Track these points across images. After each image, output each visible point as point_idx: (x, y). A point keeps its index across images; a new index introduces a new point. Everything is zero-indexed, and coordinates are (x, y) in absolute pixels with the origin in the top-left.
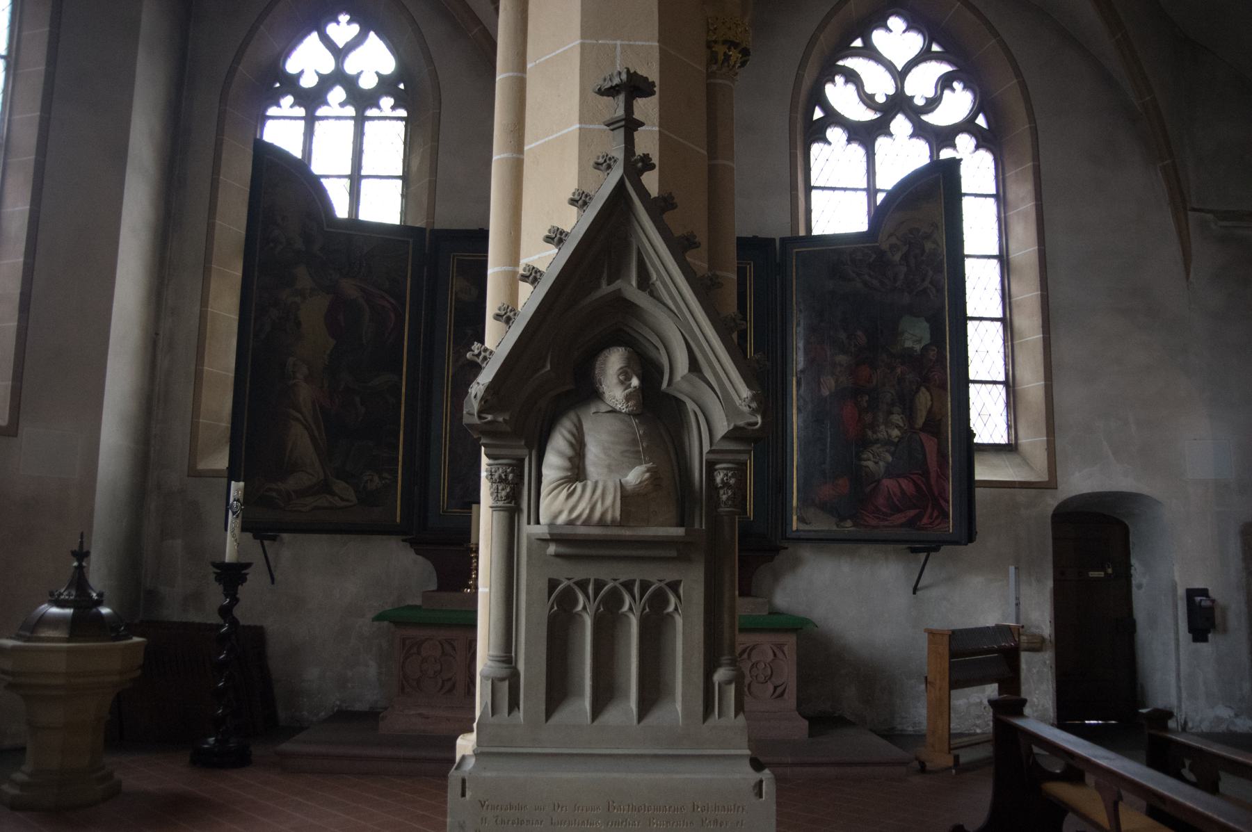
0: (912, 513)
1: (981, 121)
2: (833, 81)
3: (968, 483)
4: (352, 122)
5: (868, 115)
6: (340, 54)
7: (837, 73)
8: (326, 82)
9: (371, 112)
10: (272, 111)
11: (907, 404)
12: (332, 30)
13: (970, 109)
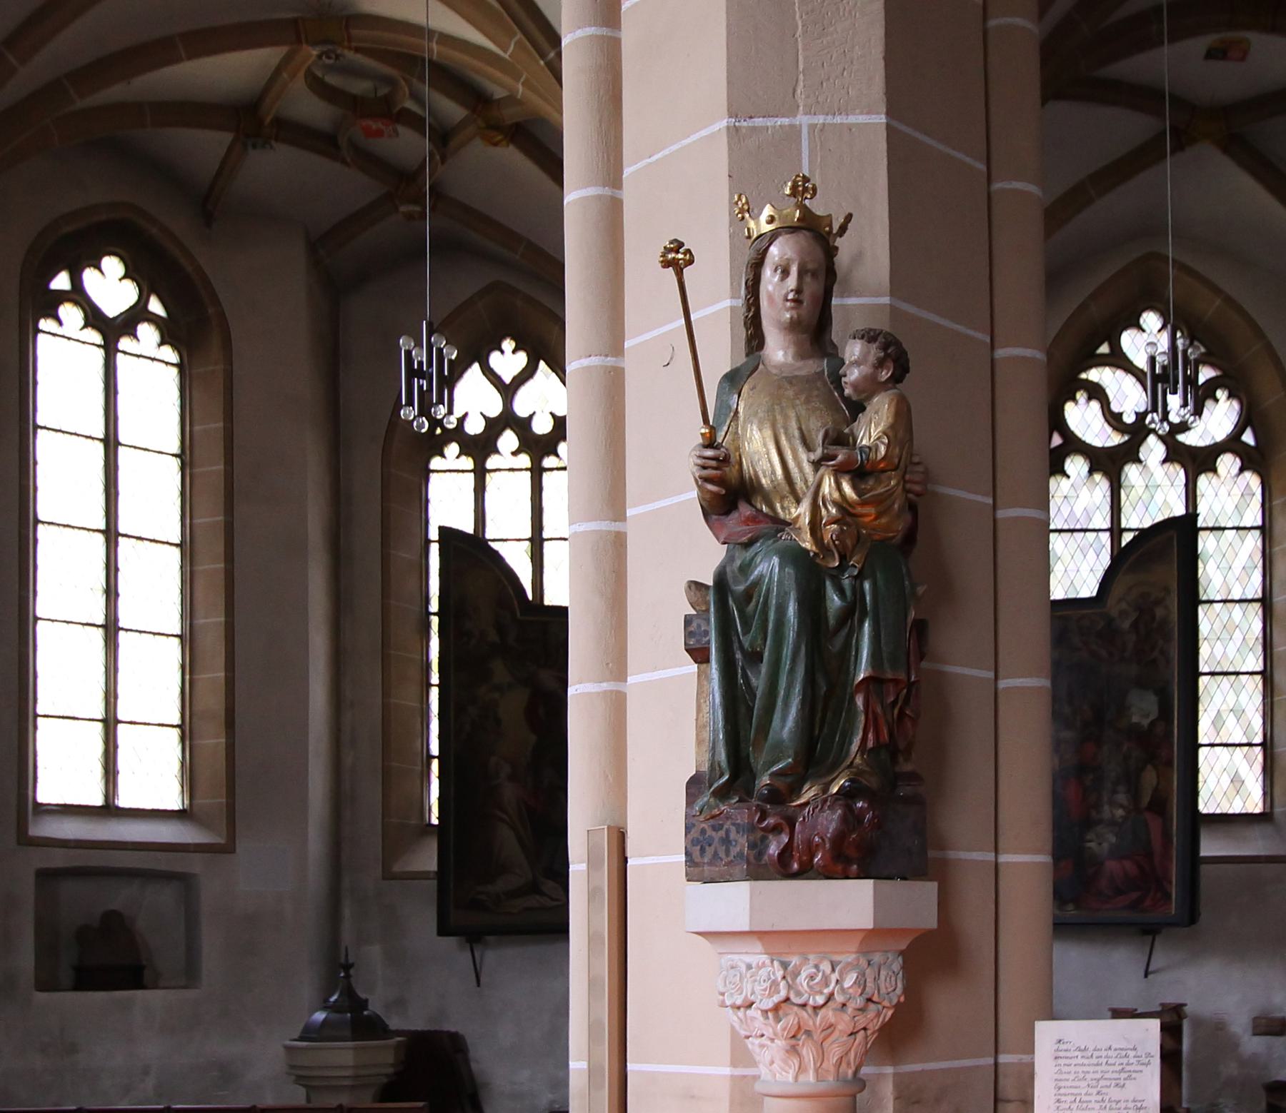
0: (1135, 895)
1: (1248, 438)
2: (1074, 399)
3: (1193, 860)
4: (528, 474)
5: (1115, 439)
6: (508, 391)
7: (1078, 389)
8: (495, 427)
9: (549, 462)
10: (436, 463)
11: (1131, 781)
12: (495, 360)
13: (1235, 423)
